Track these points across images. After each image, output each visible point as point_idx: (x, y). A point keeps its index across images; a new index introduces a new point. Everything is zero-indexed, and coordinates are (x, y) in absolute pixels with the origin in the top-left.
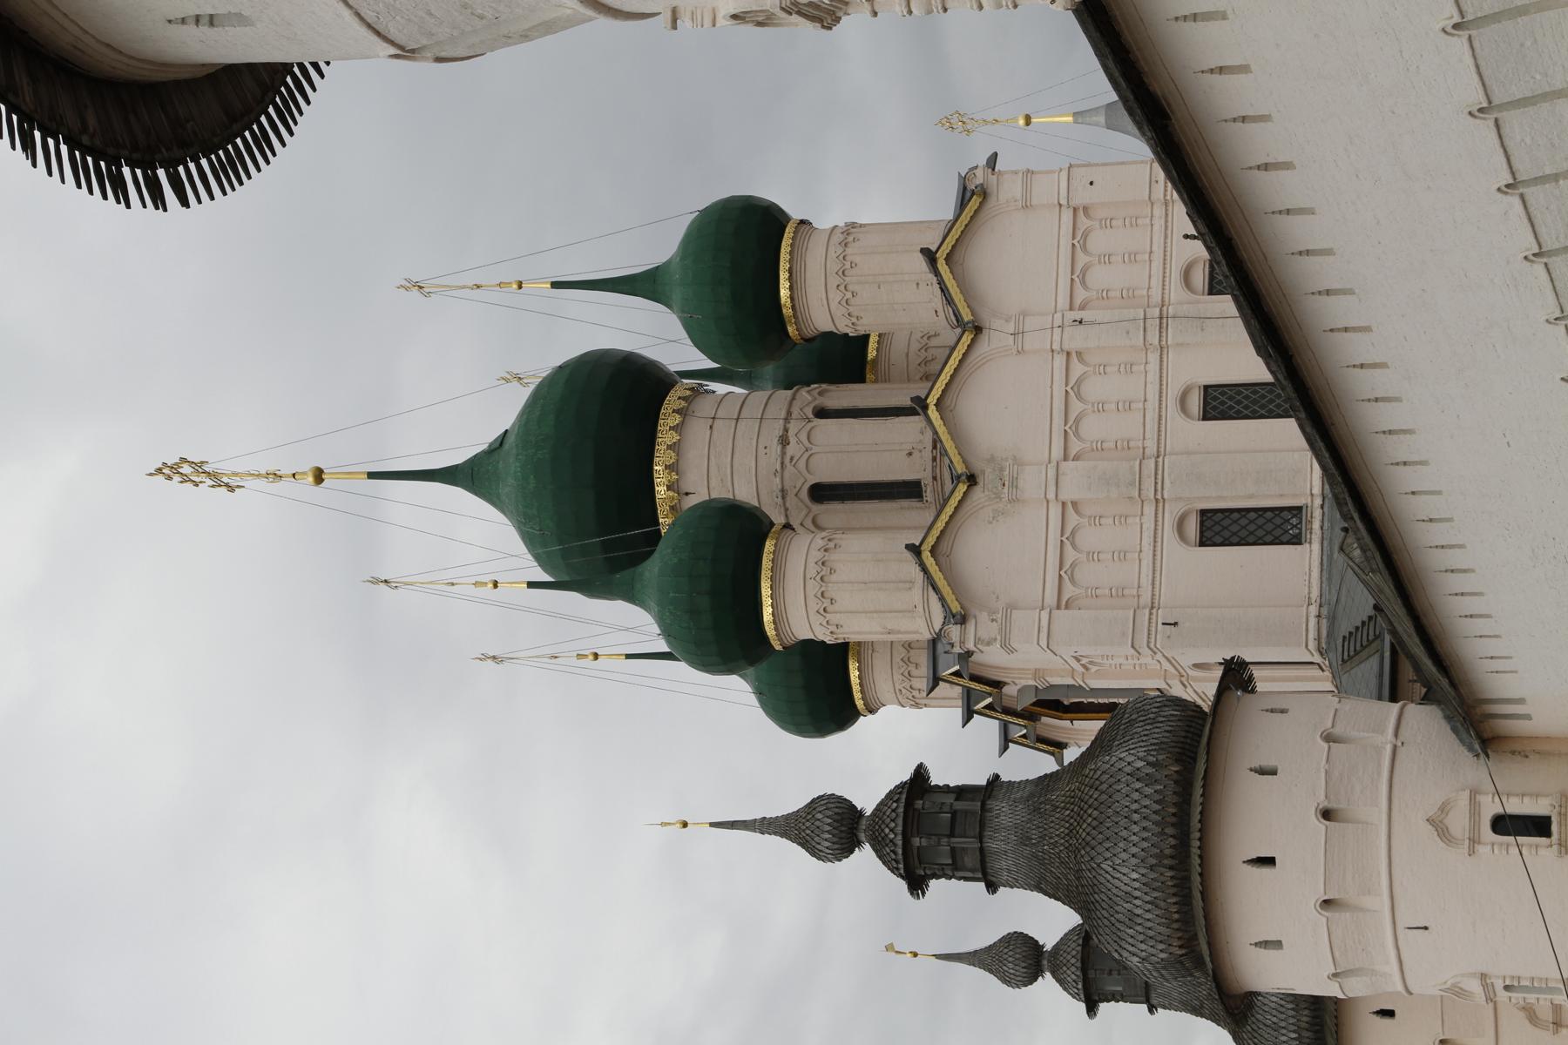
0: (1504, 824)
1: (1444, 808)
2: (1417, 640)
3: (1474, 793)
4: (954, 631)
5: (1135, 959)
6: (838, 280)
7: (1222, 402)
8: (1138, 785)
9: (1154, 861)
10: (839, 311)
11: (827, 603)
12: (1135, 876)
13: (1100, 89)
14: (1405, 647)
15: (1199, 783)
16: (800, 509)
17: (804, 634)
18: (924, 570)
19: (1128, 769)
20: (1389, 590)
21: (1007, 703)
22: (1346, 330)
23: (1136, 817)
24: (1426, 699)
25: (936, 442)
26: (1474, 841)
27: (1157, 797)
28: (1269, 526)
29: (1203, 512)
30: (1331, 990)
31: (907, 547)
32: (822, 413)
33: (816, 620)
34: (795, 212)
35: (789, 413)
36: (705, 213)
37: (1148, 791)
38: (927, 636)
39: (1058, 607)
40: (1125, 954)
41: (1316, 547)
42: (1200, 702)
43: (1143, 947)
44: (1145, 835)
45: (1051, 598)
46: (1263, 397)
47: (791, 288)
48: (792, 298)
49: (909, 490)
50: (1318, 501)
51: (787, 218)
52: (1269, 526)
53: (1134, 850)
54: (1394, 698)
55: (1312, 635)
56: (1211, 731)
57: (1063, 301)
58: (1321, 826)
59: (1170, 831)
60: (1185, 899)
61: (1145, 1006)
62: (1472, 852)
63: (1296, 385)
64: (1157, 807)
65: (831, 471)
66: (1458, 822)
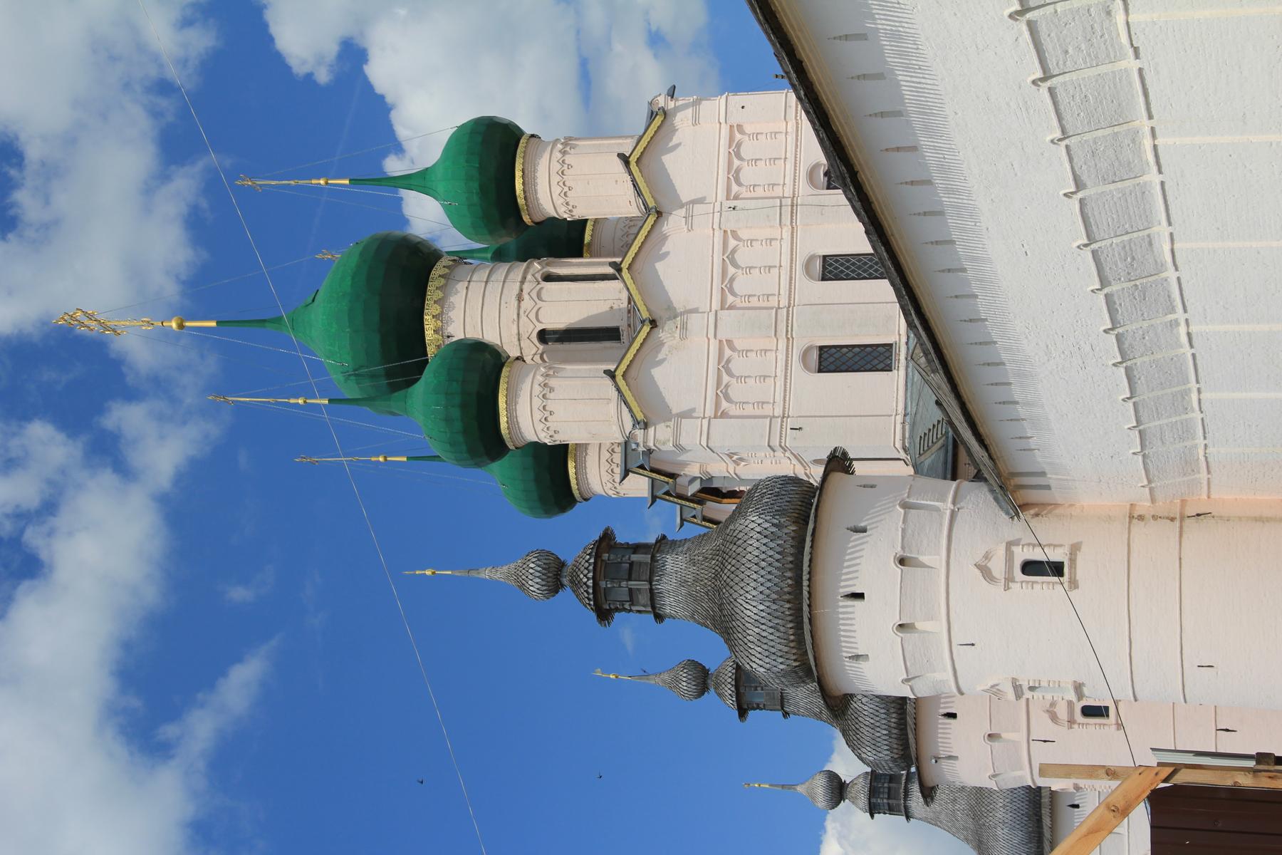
0: (1030, 568)
1: (987, 556)
2: (965, 424)
3: (1009, 545)
4: (639, 433)
5: (762, 670)
6: (558, 178)
7: (835, 268)
8: (765, 541)
9: (774, 596)
10: (559, 201)
11: (547, 414)
12: (762, 607)
13: (814, 153)
14: (968, 446)
15: (808, 539)
16: (532, 349)
17: (531, 437)
18: (619, 390)
19: (758, 529)
20: (946, 388)
21: (680, 490)
22: (898, 149)
23: (763, 564)
24: (978, 477)
25: (630, 299)
26: (1009, 579)
27: (779, 549)
28: (871, 358)
29: (821, 348)
30: (905, 692)
31: (605, 372)
32: (549, 278)
33: (540, 427)
34: (527, 128)
35: (524, 278)
36: (461, 128)
37: (772, 545)
38: (621, 440)
39: (715, 417)
40: (754, 666)
41: (902, 372)
42: (812, 481)
43: (767, 660)
44: (770, 577)
45: (710, 412)
46: (865, 264)
47: (524, 184)
48: (525, 192)
49: (611, 334)
50: (904, 339)
51: (521, 133)
52: (871, 358)
53: (762, 588)
54: (954, 478)
55: (899, 436)
56: (819, 501)
57: (721, 195)
58: (897, 570)
59: (789, 574)
60: (799, 626)
61: (780, 713)
62: (1007, 588)
63: (889, 257)
64: (778, 557)
65: (558, 319)
66: (997, 566)
